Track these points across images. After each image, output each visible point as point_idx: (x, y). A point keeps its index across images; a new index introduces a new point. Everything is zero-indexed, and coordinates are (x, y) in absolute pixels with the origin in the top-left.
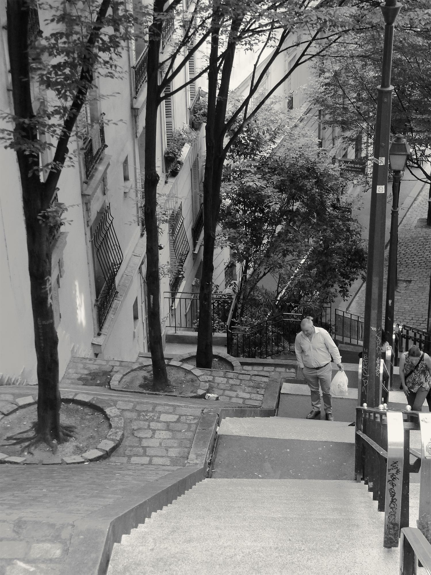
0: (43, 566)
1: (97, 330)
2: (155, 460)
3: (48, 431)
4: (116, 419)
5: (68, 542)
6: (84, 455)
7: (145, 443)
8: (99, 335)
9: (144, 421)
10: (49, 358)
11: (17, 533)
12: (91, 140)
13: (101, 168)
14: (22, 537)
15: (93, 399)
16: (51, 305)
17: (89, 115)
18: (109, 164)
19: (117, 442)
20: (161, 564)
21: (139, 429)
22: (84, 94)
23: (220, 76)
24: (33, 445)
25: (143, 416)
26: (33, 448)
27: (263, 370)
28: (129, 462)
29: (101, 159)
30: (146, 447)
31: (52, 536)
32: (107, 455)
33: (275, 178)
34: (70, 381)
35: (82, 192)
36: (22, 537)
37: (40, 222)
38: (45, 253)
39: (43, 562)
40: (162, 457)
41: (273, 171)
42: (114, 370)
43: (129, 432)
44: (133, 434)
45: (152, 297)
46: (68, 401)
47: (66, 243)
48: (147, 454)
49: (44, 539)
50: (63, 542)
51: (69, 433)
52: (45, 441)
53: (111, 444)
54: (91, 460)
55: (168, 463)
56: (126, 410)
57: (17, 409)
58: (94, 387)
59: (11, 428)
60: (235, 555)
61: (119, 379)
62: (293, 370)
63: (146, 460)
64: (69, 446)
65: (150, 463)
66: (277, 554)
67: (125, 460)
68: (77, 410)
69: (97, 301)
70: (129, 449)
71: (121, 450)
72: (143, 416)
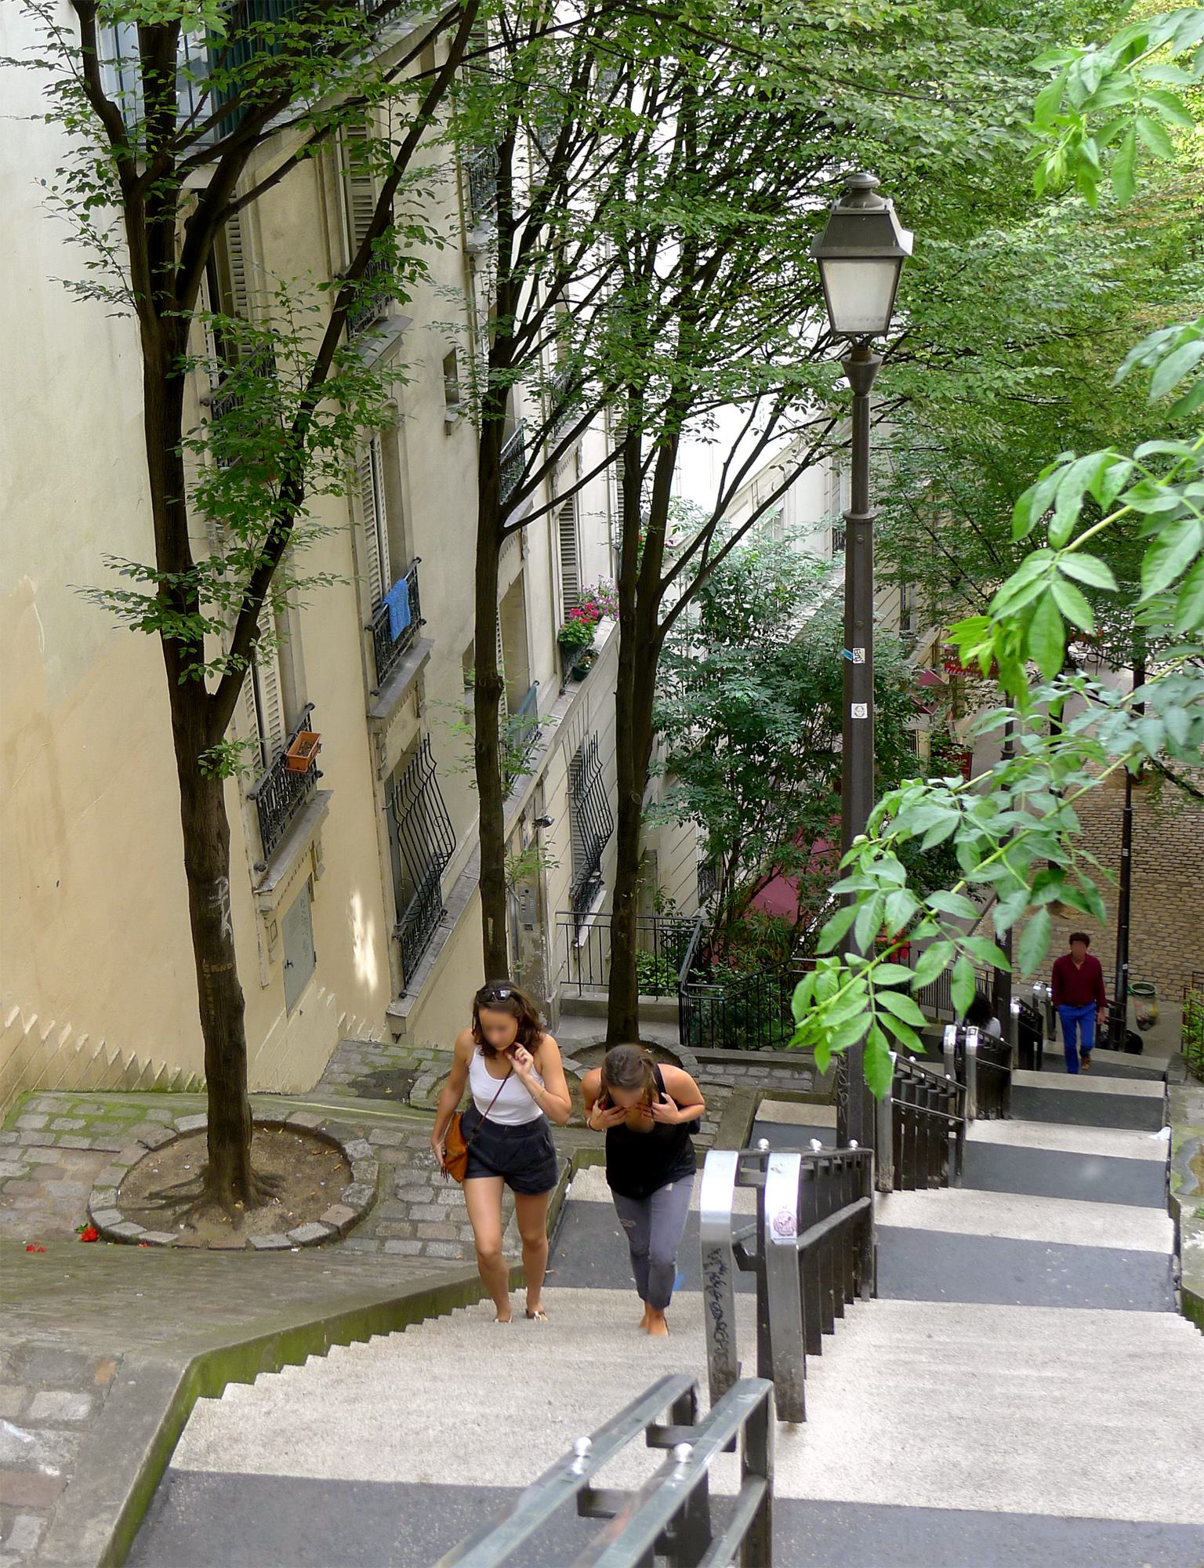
0: (49, 1434)
1: (398, 989)
2: (435, 1249)
3: (226, 1183)
4: (364, 1164)
5: (104, 1393)
6: (291, 1233)
7: (416, 1214)
8: (402, 996)
9: (421, 1168)
10: (226, 1038)
11: (14, 1370)
12: (388, 611)
13: (410, 665)
14: (21, 1379)
15: (324, 1122)
16: (229, 935)
17: (386, 562)
18: (427, 657)
19: (360, 1210)
20: (280, 1440)
21: (409, 1185)
22: (289, 522)
23: (648, 485)
24: (196, 1210)
25: (420, 1159)
26: (196, 1216)
27: (746, 1075)
28: (380, 1250)
29: (411, 647)
30: (419, 1221)
31: (78, 1379)
32: (338, 1235)
33: (789, 686)
34: (332, 1089)
35: (367, 712)
36: (21, 1379)
37: (203, 772)
38: (214, 831)
39: (51, 1427)
40: (448, 1241)
41: (786, 669)
42: (422, 1067)
43: (388, 1190)
44: (396, 1195)
45: (491, 921)
46: (261, 1124)
47: (327, 812)
48: (419, 1235)
49: (61, 1383)
50: (95, 1392)
51: (268, 1189)
52: (219, 1201)
53: (349, 1214)
54: (304, 1245)
55: (458, 1255)
56: (388, 1146)
57: (175, 1140)
58: (379, 1101)
59: (160, 1176)
60: (427, 1428)
61: (428, 1086)
62: (807, 1075)
63: (414, 1247)
64: (268, 1215)
65: (422, 1253)
66: (508, 1429)
67: (373, 1245)
68: (292, 1145)
69: (398, 928)
70: (385, 1224)
71: (367, 1226)
72: (420, 1159)
